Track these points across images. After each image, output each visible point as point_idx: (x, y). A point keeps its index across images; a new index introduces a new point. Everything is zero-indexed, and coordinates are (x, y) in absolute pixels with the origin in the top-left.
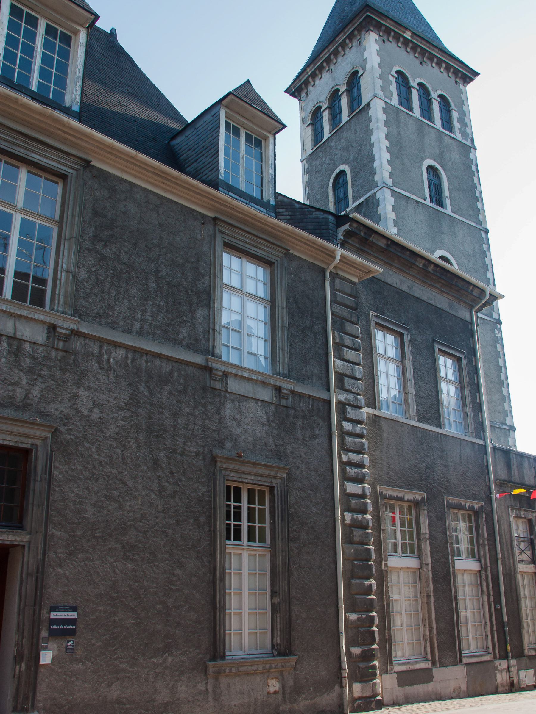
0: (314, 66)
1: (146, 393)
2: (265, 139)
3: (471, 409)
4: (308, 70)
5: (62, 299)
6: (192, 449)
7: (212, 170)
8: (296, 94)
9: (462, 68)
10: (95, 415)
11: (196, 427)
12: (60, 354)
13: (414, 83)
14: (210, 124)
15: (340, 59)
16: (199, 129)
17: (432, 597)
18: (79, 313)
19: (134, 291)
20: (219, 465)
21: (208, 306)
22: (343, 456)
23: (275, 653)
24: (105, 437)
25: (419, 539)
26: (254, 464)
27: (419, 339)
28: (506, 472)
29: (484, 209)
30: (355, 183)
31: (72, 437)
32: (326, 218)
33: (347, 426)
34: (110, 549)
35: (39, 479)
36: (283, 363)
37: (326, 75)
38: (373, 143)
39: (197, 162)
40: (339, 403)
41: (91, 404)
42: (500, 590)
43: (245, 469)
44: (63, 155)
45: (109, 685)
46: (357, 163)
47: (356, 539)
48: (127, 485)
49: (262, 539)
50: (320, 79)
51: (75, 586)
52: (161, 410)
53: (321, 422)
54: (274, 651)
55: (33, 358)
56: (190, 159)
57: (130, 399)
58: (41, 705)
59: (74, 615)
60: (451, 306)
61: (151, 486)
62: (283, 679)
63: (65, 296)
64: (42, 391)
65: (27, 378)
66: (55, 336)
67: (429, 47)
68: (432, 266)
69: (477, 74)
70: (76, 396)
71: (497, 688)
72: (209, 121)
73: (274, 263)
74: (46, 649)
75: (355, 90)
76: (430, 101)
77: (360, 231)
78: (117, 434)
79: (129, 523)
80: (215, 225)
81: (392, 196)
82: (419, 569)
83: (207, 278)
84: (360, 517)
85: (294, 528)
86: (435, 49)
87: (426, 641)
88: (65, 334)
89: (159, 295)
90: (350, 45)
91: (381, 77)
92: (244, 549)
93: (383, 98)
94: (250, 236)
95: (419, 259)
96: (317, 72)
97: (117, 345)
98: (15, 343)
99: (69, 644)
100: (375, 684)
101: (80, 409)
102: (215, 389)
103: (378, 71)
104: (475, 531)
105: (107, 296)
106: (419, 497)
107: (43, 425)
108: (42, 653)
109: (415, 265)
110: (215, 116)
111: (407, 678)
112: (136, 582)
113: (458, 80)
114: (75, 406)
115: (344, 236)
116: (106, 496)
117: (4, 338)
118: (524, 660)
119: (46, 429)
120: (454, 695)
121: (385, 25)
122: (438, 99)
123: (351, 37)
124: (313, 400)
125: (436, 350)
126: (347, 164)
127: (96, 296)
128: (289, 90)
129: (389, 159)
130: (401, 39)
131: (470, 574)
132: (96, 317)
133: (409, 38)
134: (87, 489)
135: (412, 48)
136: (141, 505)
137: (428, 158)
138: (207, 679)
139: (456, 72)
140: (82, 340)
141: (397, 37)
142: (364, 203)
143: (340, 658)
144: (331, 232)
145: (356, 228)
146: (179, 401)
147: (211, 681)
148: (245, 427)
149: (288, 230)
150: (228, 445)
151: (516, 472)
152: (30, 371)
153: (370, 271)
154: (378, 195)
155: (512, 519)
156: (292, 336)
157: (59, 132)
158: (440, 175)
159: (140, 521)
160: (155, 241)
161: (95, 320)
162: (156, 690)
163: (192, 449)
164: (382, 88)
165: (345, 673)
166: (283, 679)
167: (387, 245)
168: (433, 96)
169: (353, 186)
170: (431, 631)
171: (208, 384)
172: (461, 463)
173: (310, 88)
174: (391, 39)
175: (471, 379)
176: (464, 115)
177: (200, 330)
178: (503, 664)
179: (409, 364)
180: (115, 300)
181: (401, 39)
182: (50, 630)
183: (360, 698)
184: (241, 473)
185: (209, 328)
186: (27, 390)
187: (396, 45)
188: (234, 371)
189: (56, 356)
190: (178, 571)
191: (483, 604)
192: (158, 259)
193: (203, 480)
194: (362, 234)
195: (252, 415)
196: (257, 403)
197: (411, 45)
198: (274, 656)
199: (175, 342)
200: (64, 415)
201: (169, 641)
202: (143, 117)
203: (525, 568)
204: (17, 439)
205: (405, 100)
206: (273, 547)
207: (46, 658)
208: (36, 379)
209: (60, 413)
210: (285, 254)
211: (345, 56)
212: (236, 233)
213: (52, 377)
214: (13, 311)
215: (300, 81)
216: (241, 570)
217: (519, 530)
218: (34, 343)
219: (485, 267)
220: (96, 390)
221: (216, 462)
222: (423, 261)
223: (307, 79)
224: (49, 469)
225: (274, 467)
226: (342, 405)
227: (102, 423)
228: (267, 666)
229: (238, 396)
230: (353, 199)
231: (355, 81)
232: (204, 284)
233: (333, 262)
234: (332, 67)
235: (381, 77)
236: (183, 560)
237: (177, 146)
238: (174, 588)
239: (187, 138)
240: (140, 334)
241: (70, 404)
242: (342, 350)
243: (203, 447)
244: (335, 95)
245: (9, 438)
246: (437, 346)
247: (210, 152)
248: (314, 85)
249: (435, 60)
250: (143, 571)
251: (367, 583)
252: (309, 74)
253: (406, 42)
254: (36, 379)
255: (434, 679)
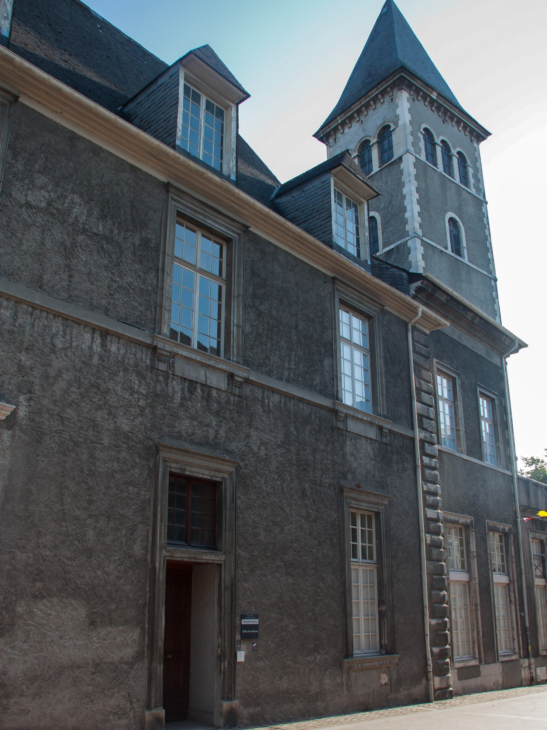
0: (345, 115)
1: (295, 433)
2: (360, 204)
3: (502, 444)
4: (338, 118)
5: (235, 351)
6: (326, 480)
7: (324, 232)
8: (324, 139)
9: (477, 128)
10: (262, 453)
11: (329, 462)
12: (237, 399)
13: (438, 141)
14: (320, 189)
15: (371, 112)
16: (306, 193)
17: (479, 606)
18: (246, 363)
19: (283, 343)
20: (345, 494)
21: (332, 356)
22: (424, 486)
23: (384, 652)
24: (270, 471)
25: (468, 557)
26: (368, 493)
27: (466, 383)
28: (526, 499)
29: (493, 259)
30: (385, 229)
31: (248, 471)
32: (400, 275)
33: (426, 460)
34: (277, 566)
35: (228, 508)
36: (383, 406)
37: (356, 126)
38: (405, 195)
39: (307, 223)
40: (421, 440)
41: (258, 443)
42: (522, 598)
43: (361, 497)
44: (229, 221)
45: (281, 679)
46: (388, 211)
47: (434, 557)
48: (285, 512)
49: (371, 558)
50: (349, 128)
51: (255, 598)
52: (305, 447)
53: (408, 456)
54: (382, 650)
55: (218, 402)
56: (299, 218)
57: (285, 438)
58: (238, 695)
59: (256, 621)
60: (487, 353)
61: (301, 513)
62: (390, 674)
63: (238, 348)
64: (226, 432)
65: (216, 420)
66: (233, 383)
67: (451, 108)
68: (478, 319)
69: (489, 134)
70: (248, 436)
71: (522, 682)
72: (318, 187)
73: (372, 317)
74: (240, 649)
75: (386, 143)
76: (450, 157)
77: (429, 287)
78: (277, 468)
79: (288, 544)
80: (334, 283)
81: (422, 245)
82: (469, 582)
83: (330, 331)
84: (435, 537)
85: (394, 547)
86: (456, 110)
87: (474, 642)
88: (240, 382)
89: (299, 346)
90: (382, 101)
91: (412, 134)
92: (360, 566)
93: (414, 154)
94: (357, 293)
95: (469, 313)
96: (347, 121)
97: (274, 391)
98: (206, 389)
99: (254, 645)
100: (448, 677)
101: (252, 447)
102: (339, 428)
103: (409, 128)
104: (505, 549)
105: (264, 347)
106: (469, 521)
107: (230, 462)
108: (238, 653)
109: (465, 317)
110: (325, 183)
111: (466, 673)
112: (295, 594)
113: (473, 139)
114: (249, 444)
115: (416, 291)
116: (273, 522)
117: (198, 385)
118: (540, 659)
119: (232, 464)
120: (494, 688)
121: (415, 85)
122: (457, 156)
123: (383, 93)
124: (403, 437)
125: (478, 393)
126: (377, 211)
127: (258, 348)
128: (317, 135)
129: (419, 211)
130: (428, 99)
131: (502, 586)
132: (259, 366)
133: (435, 98)
134: (260, 515)
135: (436, 108)
136: (296, 529)
137: (450, 211)
138: (342, 673)
139: (472, 131)
140: (250, 387)
141: (425, 97)
142: (395, 250)
143: (425, 656)
144: (405, 287)
145: (426, 285)
146: (316, 440)
147: (345, 675)
148: (360, 461)
149: (385, 289)
150: (350, 476)
151: (533, 499)
152: (217, 414)
153: (439, 324)
154: (410, 244)
155: (531, 540)
156: (387, 382)
157: (228, 201)
158: (458, 227)
159: (295, 542)
160: (294, 298)
161: (258, 369)
162: (310, 683)
163: (326, 480)
164: (413, 145)
165: (430, 669)
166: (390, 674)
167: (447, 300)
168: (453, 153)
169: (383, 233)
170: (478, 634)
171: (335, 425)
172: (496, 491)
173: (339, 135)
174: (419, 98)
175: (502, 418)
176: (478, 171)
177: (327, 377)
178: (525, 662)
179: (460, 404)
180: (271, 351)
181: (428, 99)
182: (241, 634)
183: (439, 689)
184: (358, 501)
185: (333, 375)
186: (216, 431)
187: (423, 104)
188: (352, 413)
189: (234, 401)
190: (321, 585)
191: (511, 612)
192: (297, 314)
193: (334, 507)
194: (430, 290)
195: (363, 451)
196: (367, 441)
197: (436, 105)
198: (382, 655)
199: (311, 388)
200: (242, 452)
201: (317, 642)
202: (249, 174)
203: (539, 582)
204: (212, 473)
205: (431, 156)
206: (380, 562)
207: (241, 656)
208: (221, 421)
209: (239, 451)
210: (381, 310)
211: (376, 110)
212: (349, 291)
213: (232, 419)
214: (204, 362)
215: (329, 127)
216: (358, 583)
217: (535, 549)
218: (219, 390)
219: (496, 313)
220: (262, 431)
221: (343, 491)
222: (472, 315)
223: (337, 127)
224: (234, 499)
225: (381, 496)
226: (422, 441)
227: (267, 459)
228: (381, 662)
229: (354, 435)
230: (383, 245)
231: (386, 134)
232: (328, 336)
233: (415, 317)
234: (363, 118)
235: (412, 134)
236: (324, 575)
237: (283, 205)
238: (319, 598)
239: (293, 199)
240: (288, 381)
241: (245, 443)
242: (421, 394)
243: (333, 478)
244: (365, 145)
245: (206, 472)
246: (479, 389)
247: (321, 216)
248: (343, 132)
249: (455, 119)
250: (299, 585)
251: (442, 593)
252: (339, 122)
253: (432, 102)
254: (221, 421)
255: (482, 674)
